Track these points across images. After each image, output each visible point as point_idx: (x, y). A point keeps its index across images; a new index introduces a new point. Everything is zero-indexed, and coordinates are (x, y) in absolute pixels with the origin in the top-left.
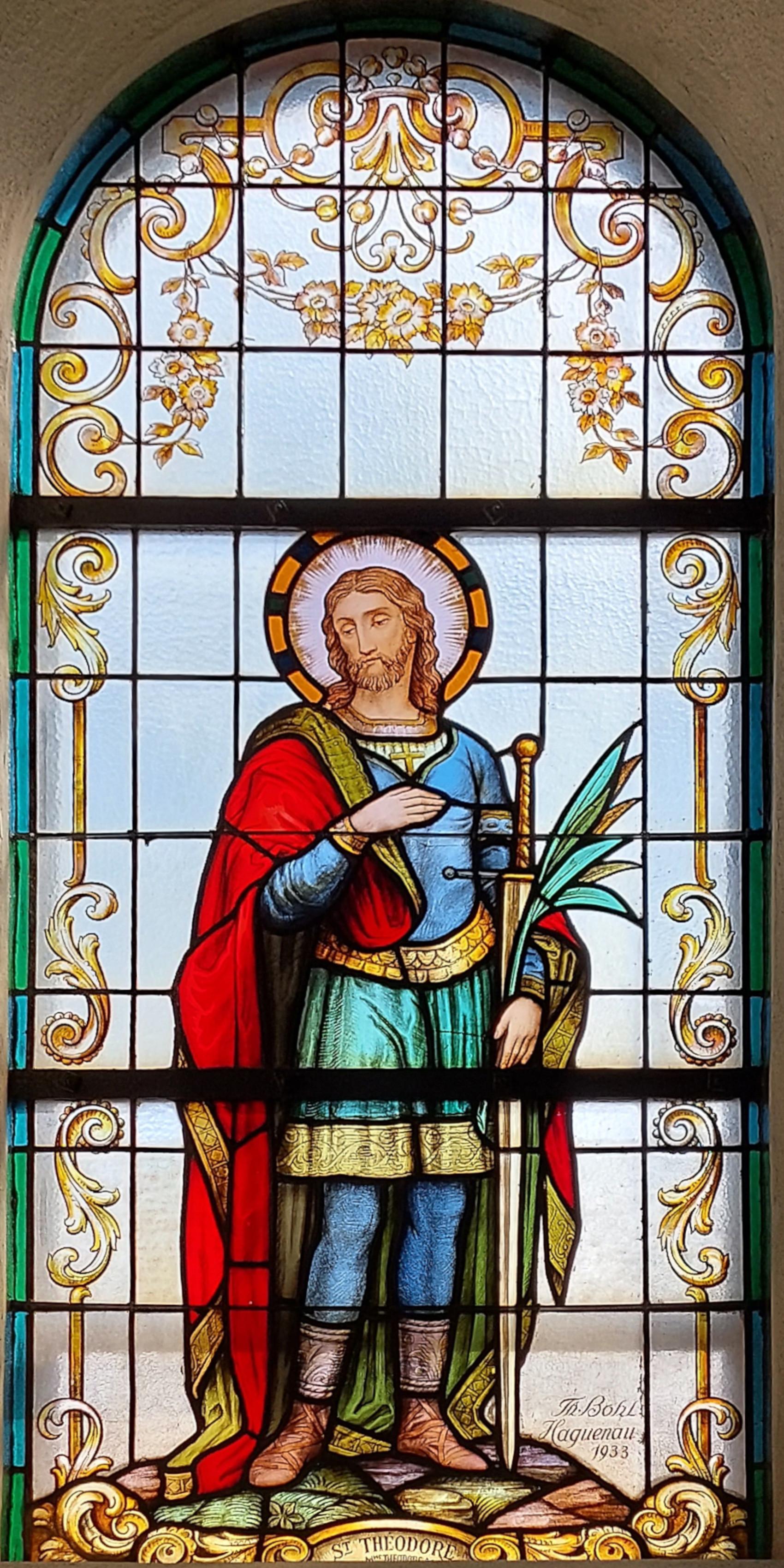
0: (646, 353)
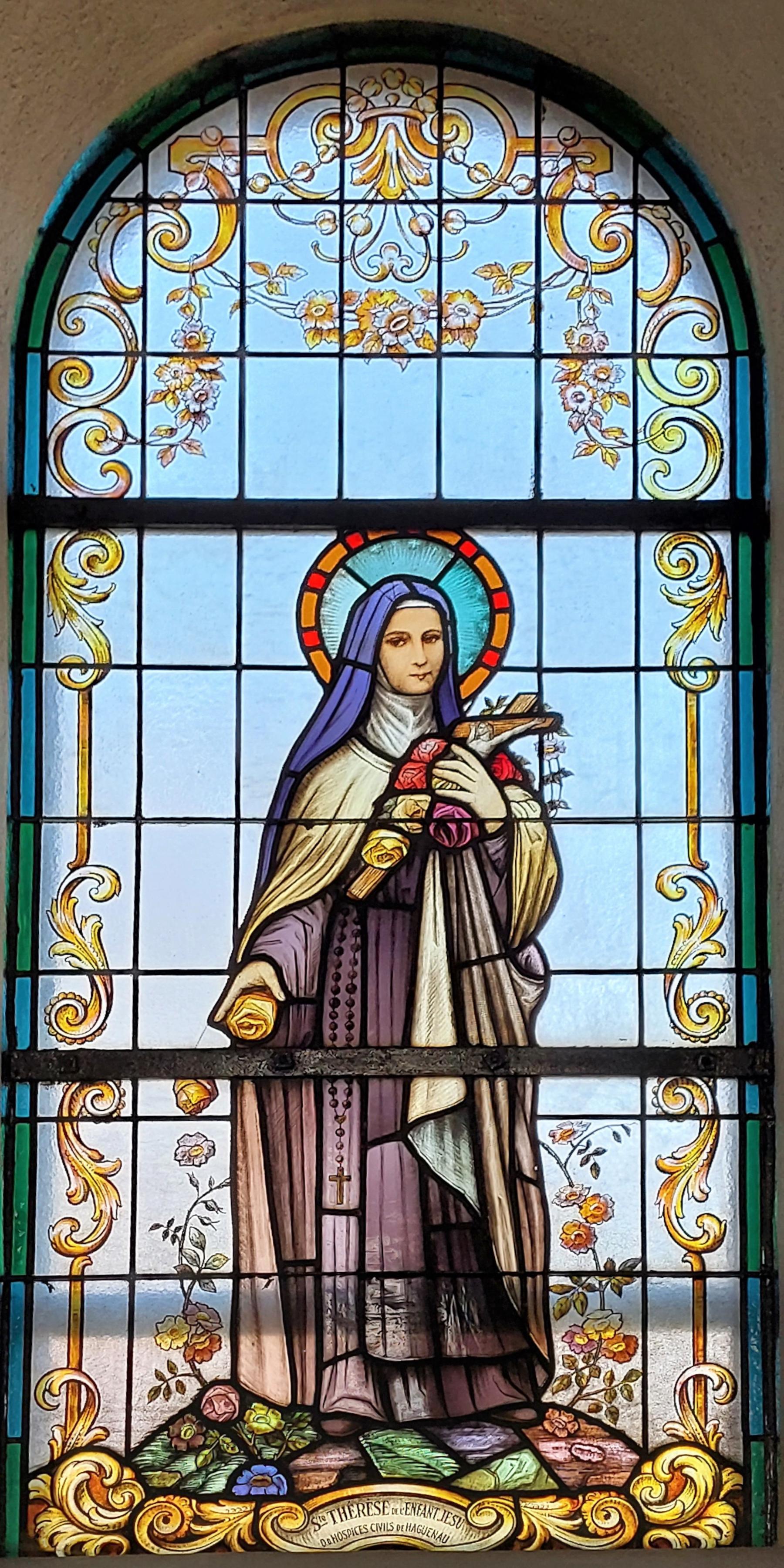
0: (634, 355)
